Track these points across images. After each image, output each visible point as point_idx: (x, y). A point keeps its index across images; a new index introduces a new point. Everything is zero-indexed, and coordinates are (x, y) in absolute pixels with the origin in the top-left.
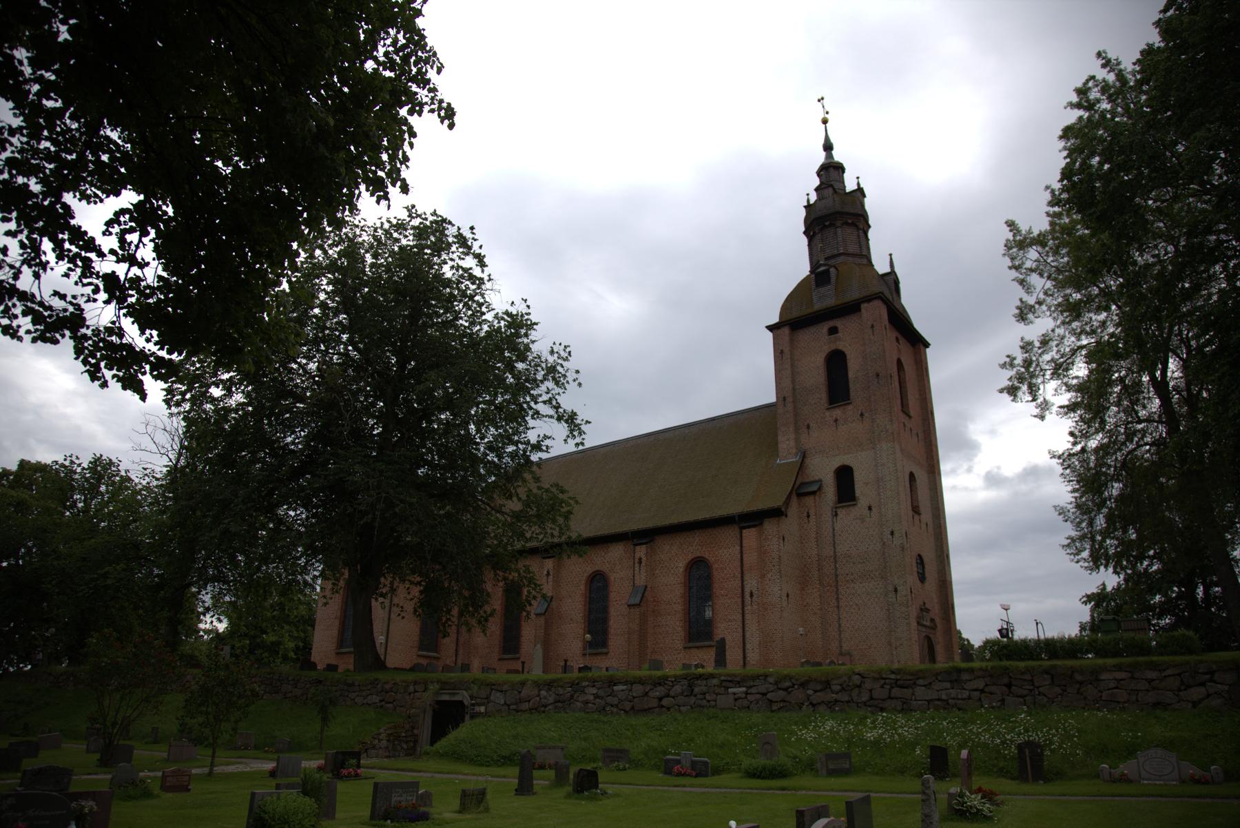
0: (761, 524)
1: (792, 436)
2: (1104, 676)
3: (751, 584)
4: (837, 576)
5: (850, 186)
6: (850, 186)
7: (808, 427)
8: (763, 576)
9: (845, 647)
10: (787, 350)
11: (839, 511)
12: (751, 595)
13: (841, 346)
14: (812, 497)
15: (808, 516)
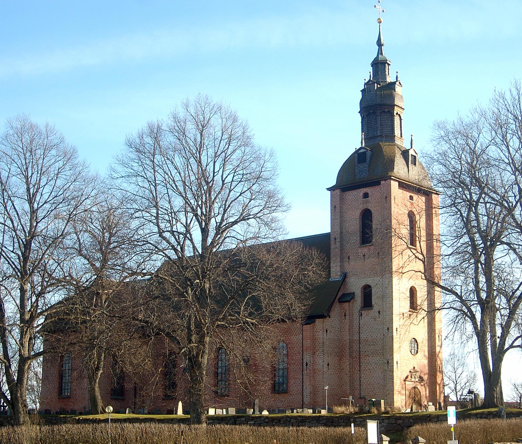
0: (314, 322)
1: (339, 264)
2: (357, 420)
3: (307, 358)
4: (360, 352)
5: (390, 79)
6: (390, 79)
7: (349, 258)
8: (314, 354)
9: (363, 394)
10: (338, 206)
11: (363, 312)
12: (307, 365)
13: (370, 206)
14: (347, 304)
15: (345, 315)
